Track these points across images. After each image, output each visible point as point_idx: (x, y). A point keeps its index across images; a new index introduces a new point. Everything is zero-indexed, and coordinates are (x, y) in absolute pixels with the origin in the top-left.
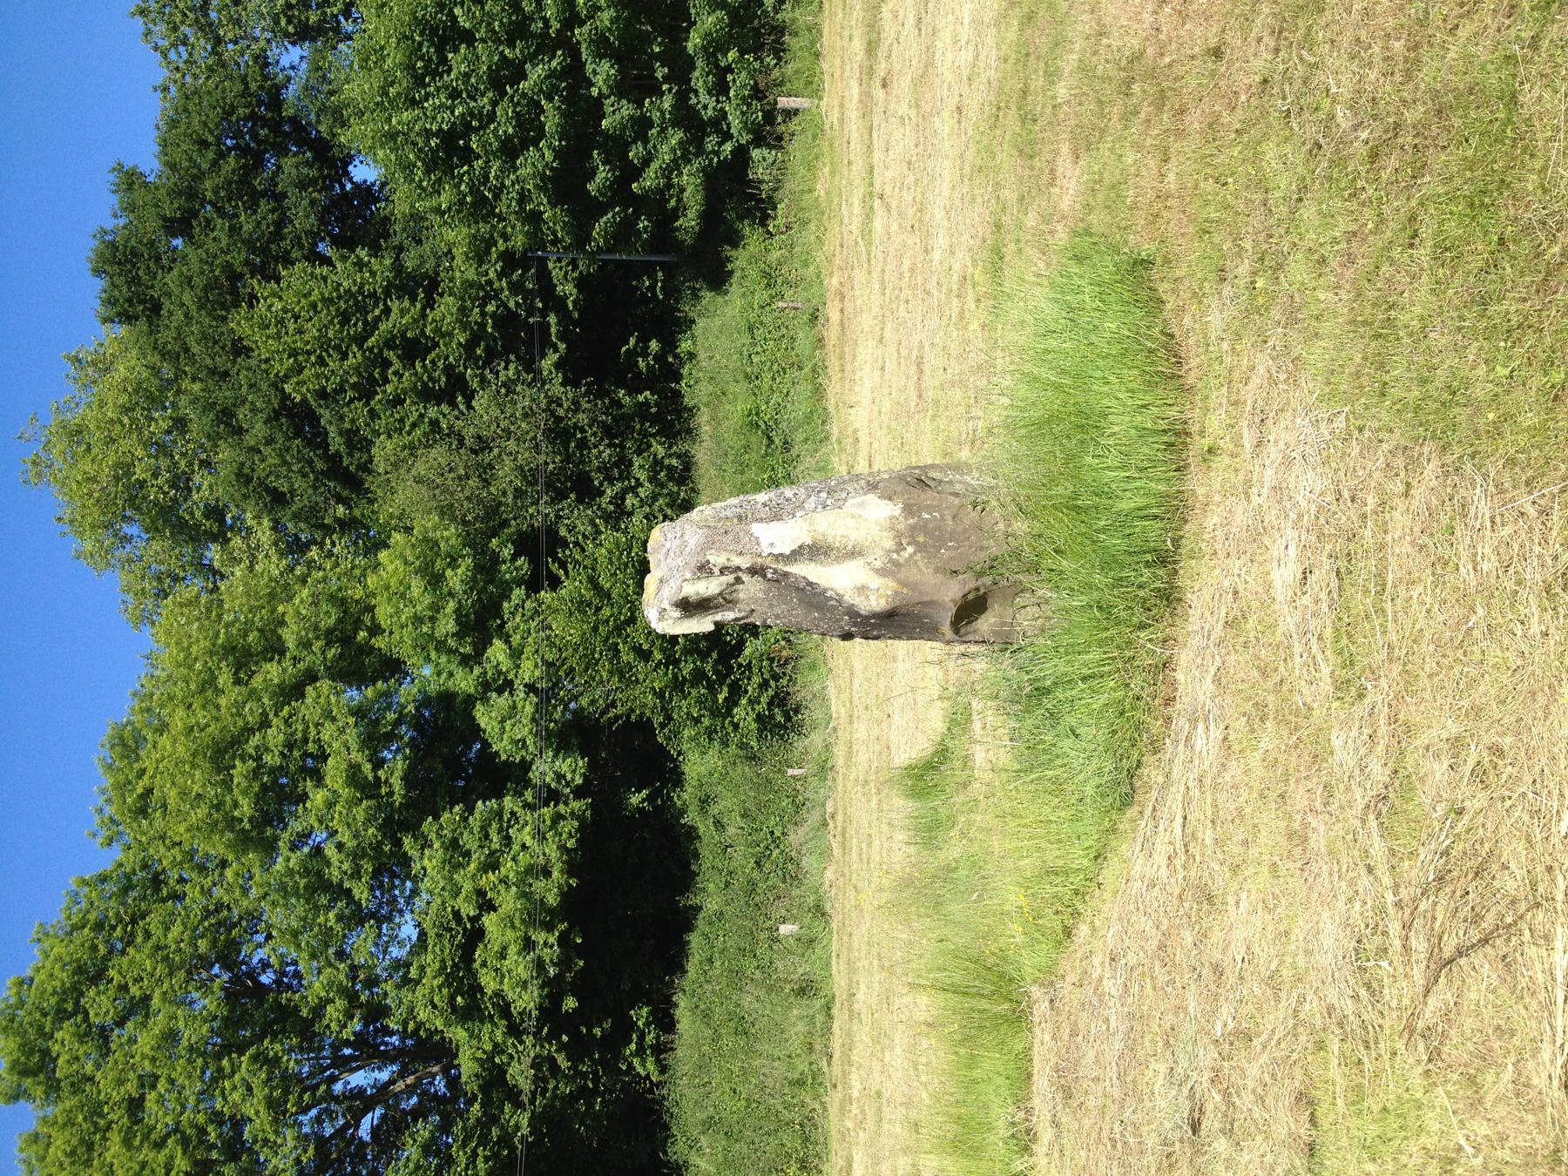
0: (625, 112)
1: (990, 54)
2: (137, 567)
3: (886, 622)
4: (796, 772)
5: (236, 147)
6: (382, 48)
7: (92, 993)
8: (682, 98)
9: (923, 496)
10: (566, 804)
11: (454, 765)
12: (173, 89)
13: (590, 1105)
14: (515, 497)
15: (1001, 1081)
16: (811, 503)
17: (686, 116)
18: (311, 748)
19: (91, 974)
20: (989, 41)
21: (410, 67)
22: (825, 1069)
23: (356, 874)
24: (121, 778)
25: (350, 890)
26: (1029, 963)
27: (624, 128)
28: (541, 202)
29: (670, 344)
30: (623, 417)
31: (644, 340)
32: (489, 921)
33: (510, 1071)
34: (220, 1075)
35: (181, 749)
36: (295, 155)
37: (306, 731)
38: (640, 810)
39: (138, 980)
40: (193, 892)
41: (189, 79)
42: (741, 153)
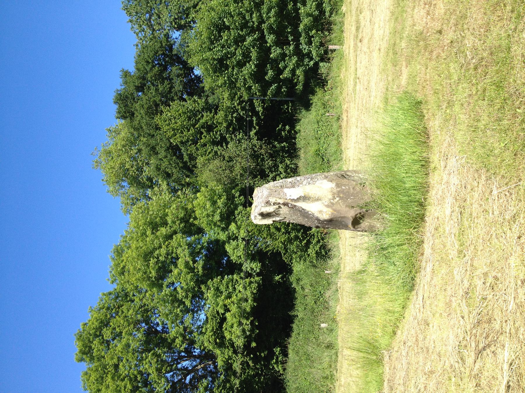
0: (278, 52)
1: (387, 32)
2: (126, 196)
3: (330, 223)
4: (328, 272)
5: (158, 64)
6: (201, 32)
7: (105, 330)
8: (297, 46)
9: (343, 181)
10: (254, 278)
11: (219, 263)
12: (140, 45)
13: (260, 379)
14: (241, 176)
15: (374, 382)
16: (304, 183)
17: (298, 52)
18: (174, 255)
19: (104, 323)
20: (387, 27)
21: (210, 38)
22: (335, 374)
23: (187, 297)
24: (117, 262)
25: (184, 302)
26: (383, 342)
27: (278, 57)
28: (250, 82)
29: (293, 127)
30: (277, 151)
31: (284, 125)
32: (228, 315)
33: (234, 365)
34: (142, 359)
35: (134, 254)
36: (176, 66)
37: (172, 250)
38: (279, 282)
39: (119, 326)
40: (137, 300)
41: (144, 42)
42: (316, 64)
